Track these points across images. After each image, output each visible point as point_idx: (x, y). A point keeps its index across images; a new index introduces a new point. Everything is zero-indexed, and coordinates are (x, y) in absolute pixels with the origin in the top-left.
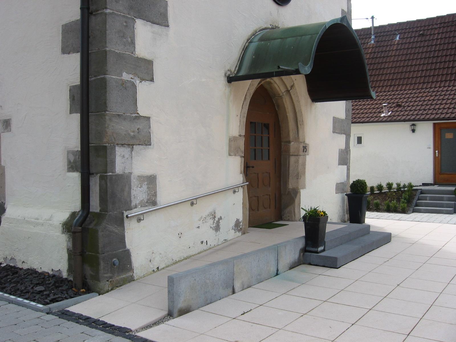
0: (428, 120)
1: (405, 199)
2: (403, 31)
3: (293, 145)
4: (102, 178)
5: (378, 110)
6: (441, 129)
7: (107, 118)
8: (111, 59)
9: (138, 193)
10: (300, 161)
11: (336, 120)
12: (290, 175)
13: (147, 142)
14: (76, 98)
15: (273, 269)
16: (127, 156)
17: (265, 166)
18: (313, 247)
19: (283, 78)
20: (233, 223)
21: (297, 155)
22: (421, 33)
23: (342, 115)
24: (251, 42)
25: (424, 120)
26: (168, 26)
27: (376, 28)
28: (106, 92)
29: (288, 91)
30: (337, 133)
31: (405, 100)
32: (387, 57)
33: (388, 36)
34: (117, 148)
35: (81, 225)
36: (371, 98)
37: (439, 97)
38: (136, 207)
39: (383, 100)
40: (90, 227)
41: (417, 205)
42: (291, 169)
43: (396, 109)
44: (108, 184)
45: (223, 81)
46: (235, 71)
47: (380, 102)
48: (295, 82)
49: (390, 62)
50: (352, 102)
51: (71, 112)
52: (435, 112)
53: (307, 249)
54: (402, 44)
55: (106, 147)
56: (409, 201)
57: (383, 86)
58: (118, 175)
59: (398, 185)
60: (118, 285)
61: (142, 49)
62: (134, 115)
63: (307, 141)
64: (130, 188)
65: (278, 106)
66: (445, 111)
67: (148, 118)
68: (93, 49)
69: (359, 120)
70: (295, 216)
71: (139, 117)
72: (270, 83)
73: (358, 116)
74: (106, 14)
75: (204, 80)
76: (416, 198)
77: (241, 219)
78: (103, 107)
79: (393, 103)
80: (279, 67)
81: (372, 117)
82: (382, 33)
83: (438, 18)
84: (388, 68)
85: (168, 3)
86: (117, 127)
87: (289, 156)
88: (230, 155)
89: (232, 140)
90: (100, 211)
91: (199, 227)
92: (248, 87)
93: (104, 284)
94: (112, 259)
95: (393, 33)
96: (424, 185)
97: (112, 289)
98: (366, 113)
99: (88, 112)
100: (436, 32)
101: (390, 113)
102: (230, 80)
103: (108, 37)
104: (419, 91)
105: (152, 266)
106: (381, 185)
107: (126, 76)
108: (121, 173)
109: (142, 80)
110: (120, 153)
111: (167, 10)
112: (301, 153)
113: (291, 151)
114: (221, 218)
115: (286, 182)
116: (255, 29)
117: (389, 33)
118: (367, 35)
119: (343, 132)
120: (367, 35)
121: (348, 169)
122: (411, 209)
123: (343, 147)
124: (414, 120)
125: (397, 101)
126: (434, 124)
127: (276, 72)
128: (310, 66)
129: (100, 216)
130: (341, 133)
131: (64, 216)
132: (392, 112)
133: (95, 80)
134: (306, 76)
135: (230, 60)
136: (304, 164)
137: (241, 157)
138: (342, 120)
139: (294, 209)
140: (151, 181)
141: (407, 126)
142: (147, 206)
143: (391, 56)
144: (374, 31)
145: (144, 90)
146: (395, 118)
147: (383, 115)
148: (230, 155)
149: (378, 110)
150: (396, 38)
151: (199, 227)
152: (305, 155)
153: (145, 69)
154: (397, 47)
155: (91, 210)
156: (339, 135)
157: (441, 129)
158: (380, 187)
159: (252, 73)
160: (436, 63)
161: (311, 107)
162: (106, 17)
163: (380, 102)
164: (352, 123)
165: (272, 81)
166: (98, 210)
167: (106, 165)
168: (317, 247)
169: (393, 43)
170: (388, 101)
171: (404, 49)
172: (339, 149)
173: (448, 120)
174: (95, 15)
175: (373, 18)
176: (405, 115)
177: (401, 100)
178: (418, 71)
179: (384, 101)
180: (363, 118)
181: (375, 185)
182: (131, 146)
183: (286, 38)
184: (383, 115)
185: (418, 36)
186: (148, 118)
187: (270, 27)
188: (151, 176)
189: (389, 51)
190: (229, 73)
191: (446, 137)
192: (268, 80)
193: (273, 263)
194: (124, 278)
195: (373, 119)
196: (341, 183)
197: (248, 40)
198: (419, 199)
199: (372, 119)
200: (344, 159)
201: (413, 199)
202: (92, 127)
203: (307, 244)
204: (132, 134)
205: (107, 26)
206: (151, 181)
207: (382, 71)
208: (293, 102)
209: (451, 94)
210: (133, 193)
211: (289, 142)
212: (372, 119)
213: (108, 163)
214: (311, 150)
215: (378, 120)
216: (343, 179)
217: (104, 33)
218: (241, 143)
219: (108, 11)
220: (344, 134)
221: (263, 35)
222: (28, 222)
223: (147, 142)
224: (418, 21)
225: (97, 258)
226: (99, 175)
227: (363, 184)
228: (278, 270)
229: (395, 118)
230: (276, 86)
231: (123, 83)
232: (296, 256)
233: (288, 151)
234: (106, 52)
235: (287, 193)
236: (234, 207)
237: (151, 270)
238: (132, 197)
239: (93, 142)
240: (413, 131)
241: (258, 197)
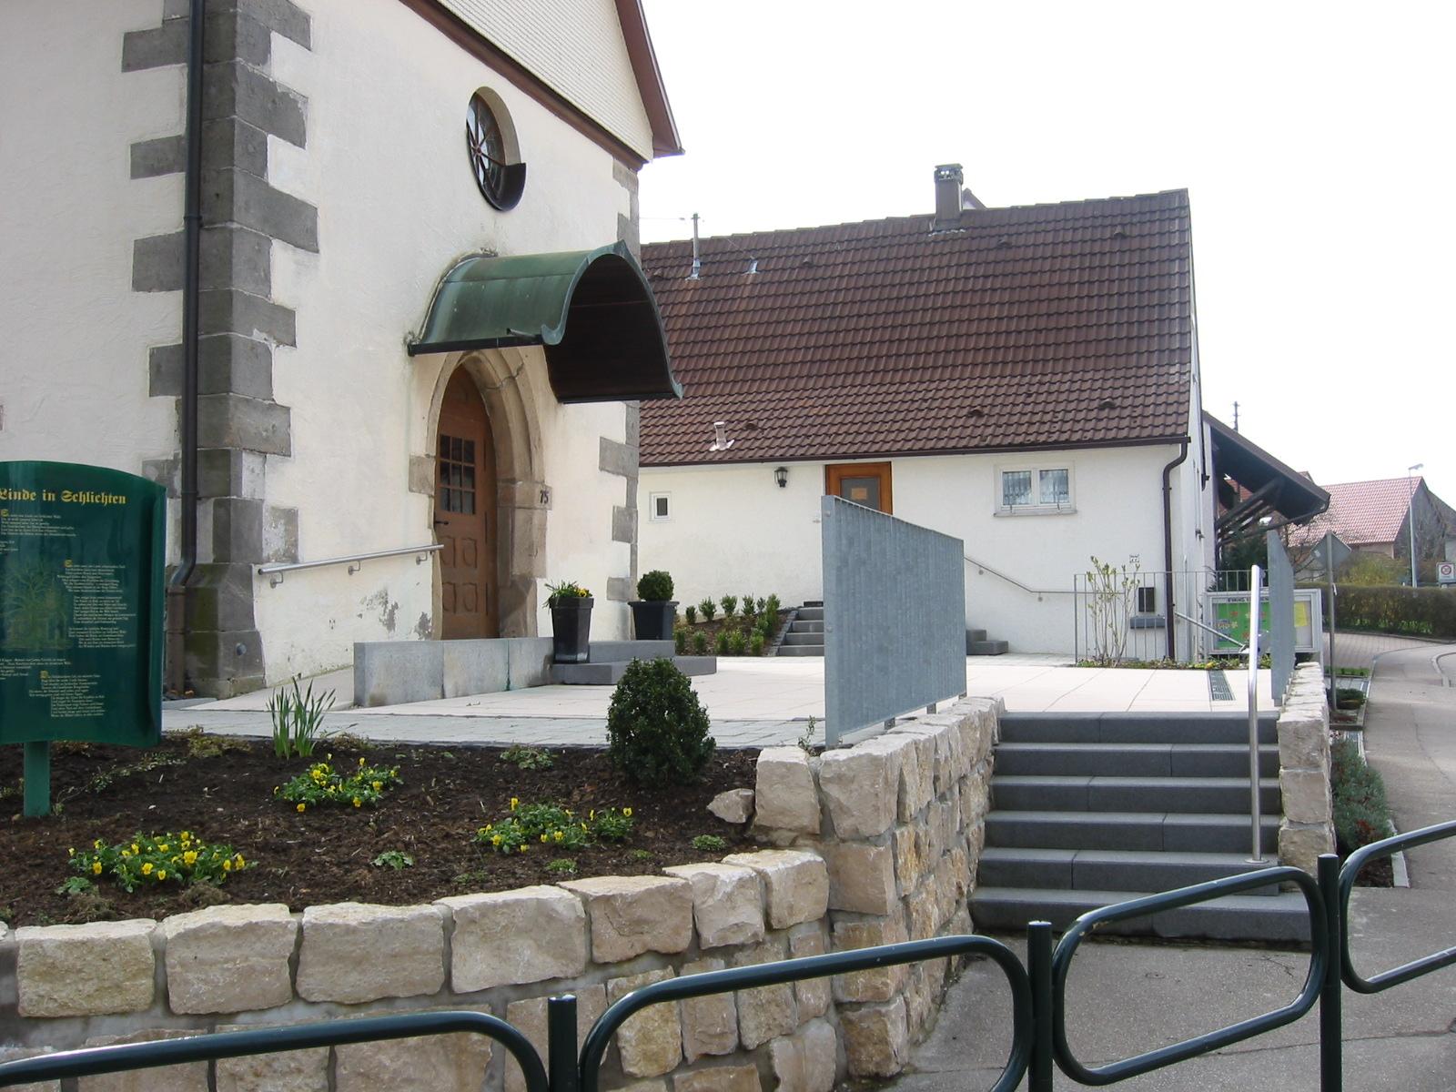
0: (813, 458)
1: (761, 628)
2: (767, 254)
4: (218, 504)
5: (705, 437)
6: (841, 479)
7: (231, 402)
8: (238, 306)
9: (272, 538)
10: (536, 521)
11: (605, 445)
12: (516, 546)
14: (163, 369)
15: (502, 678)
16: (257, 471)
17: (468, 525)
18: (567, 654)
19: (503, 350)
20: (416, 622)
21: (529, 508)
22: (806, 260)
23: (619, 435)
24: (448, 282)
25: (803, 458)
26: (317, 252)
27: (702, 242)
28: (230, 360)
29: (512, 378)
30: (608, 471)
31: (767, 414)
32: (729, 313)
33: (732, 265)
35: (184, 582)
36: (675, 396)
37: (929, 433)
38: (268, 561)
39: (718, 413)
40: (201, 585)
41: (786, 642)
42: (518, 534)
43: (744, 434)
44: (232, 514)
45: (401, 351)
46: (420, 333)
47: (709, 418)
48: (526, 361)
49: (734, 326)
50: (642, 409)
51: (153, 392)
52: (827, 440)
53: (558, 657)
54: (763, 284)
55: (229, 451)
56: (770, 634)
57: (717, 383)
58: (244, 501)
59: (748, 602)
60: (243, 690)
61: (281, 291)
62: (267, 402)
63: (548, 482)
64: (261, 527)
65: (492, 408)
66: (850, 438)
67: (288, 409)
68: (205, 288)
69: (661, 458)
70: (526, 629)
71: (274, 406)
72: (477, 360)
73: (659, 449)
74: (231, 231)
75: (370, 349)
76: (786, 627)
77: (429, 616)
78: (225, 384)
79: (739, 421)
80: (509, 331)
81: (690, 453)
82: (717, 254)
83: (845, 227)
84: (729, 340)
85: (319, 211)
86: (245, 421)
87: (514, 509)
88: (411, 490)
89: (414, 462)
90: (214, 561)
91: (361, 616)
92: (442, 364)
93: (224, 684)
94: (235, 642)
95: (742, 256)
96: (807, 604)
97: (234, 696)
98: (677, 443)
99: (196, 394)
100: (840, 260)
101: (730, 444)
102: (414, 350)
103: (236, 269)
104: (797, 394)
105: (290, 669)
106: (710, 603)
107: (258, 336)
108: (249, 498)
109: (280, 343)
110: (249, 463)
112: (538, 504)
113: (517, 499)
114: (396, 607)
115: (508, 563)
116: (454, 256)
117: (733, 257)
118: (683, 257)
119: (621, 471)
120: (683, 257)
121: (634, 552)
122: (775, 649)
123: (623, 503)
124: (782, 458)
125: (747, 416)
126: (827, 467)
127: (500, 339)
128: (561, 330)
129: (216, 570)
130: (618, 474)
132: (736, 440)
133: (208, 339)
134: (551, 352)
135: (411, 314)
136: (543, 528)
137: (430, 496)
138: (620, 446)
139: (525, 616)
140: (290, 517)
141: (767, 472)
142: (283, 562)
143: (738, 312)
144: (700, 249)
145: (281, 359)
146: (741, 454)
147: (714, 448)
149: (705, 437)
150: (749, 268)
151: (361, 616)
152: (545, 510)
153: (283, 324)
154: (751, 291)
155: (198, 562)
156: (614, 477)
157: (841, 480)
158: (708, 609)
159: (453, 339)
160: (837, 332)
161: (556, 413)
162: (231, 235)
163: (709, 418)
164: (642, 465)
165: (481, 357)
167: (229, 484)
168: (575, 652)
169: (743, 282)
170: (728, 417)
171: (768, 296)
174: (207, 230)
175: (695, 217)
176: (762, 447)
177: (757, 415)
178: (797, 349)
179: (719, 417)
180: (670, 453)
181: (696, 603)
183: (517, 278)
184: (714, 448)
185: (800, 268)
186: (288, 409)
187: (481, 252)
188: (290, 510)
189: (733, 299)
190: (410, 337)
192: (475, 354)
193: (501, 665)
194: (252, 680)
195: (693, 456)
196: (618, 579)
197: (442, 278)
198: (791, 630)
199: (690, 457)
200: (624, 528)
201: (780, 629)
203: (556, 649)
205: (234, 252)
206: (290, 517)
207: (879, 333)
208: (521, 401)
209: (956, 425)
210: (265, 535)
211: (513, 481)
212: (690, 457)
213: (229, 481)
214: (557, 498)
215: (704, 457)
216: (624, 571)
217: (227, 262)
218: (430, 470)
219: (235, 226)
220: (623, 475)
221: (469, 270)
223: (285, 452)
225: (215, 637)
226: (213, 499)
227: (664, 579)
228: (509, 682)
229: (741, 454)
230: (488, 365)
231: (254, 346)
232: (540, 667)
233: (510, 498)
234: (230, 293)
235: (509, 584)
236: (417, 590)
237: (289, 676)
238: (264, 542)
240: (782, 483)
241: (454, 585)
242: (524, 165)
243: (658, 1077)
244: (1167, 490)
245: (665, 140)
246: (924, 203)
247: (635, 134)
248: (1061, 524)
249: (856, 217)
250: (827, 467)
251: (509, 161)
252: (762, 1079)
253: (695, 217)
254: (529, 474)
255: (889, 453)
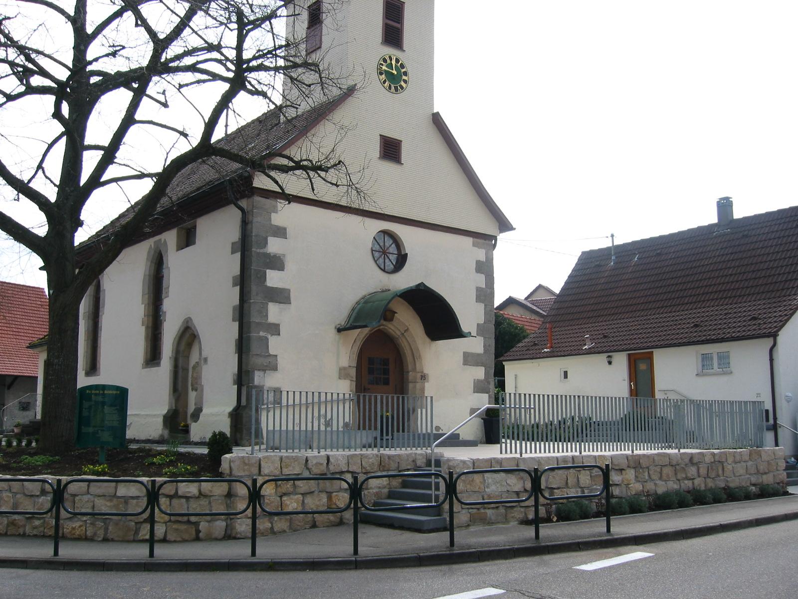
3: (411, 375)
13: (275, 368)
34: (256, 372)
67: (276, 356)
71: (270, 355)
74: (250, 303)
78: (249, 350)
86: (255, 361)
88: (340, 378)
92: (358, 335)
102: (339, 330)
107: (262, 334)
109: (272, 335)
111: (289, 294)
112: (419, 380)
116: (364, 294)
126: (629, 355)
131: (230, 409)
132: (596, 343)
138: (479, 355)
140: (277, 391)
141: (603, 358)
145: (273, 341)
148: (340, 378)
153: (275, 329)
166: (245, 404)
172: (475, 380)
173: (635, 350)
175: (612, 236)
182: (264, 371)
186: (276, 356)
191: (641, 368)
202: (244, 360)
204: (265, 364)
211: (408, 372)
222: (213, 415)
224: (780, 212)
231: (260, 337)
239: (244, 367)
240: (610, 363)
242: (407, 254)
243: (163, 523)
244: (771, 360)
245: (505, 225)
246: (710, 217)
247: (485, 226)
248: (724, 379)
249: (638, 238)
250: (629, 354)
251: (403, 253)
252: (196, 530)
253: (612, 236)
254: (414, 369)
255: (653, 347)
